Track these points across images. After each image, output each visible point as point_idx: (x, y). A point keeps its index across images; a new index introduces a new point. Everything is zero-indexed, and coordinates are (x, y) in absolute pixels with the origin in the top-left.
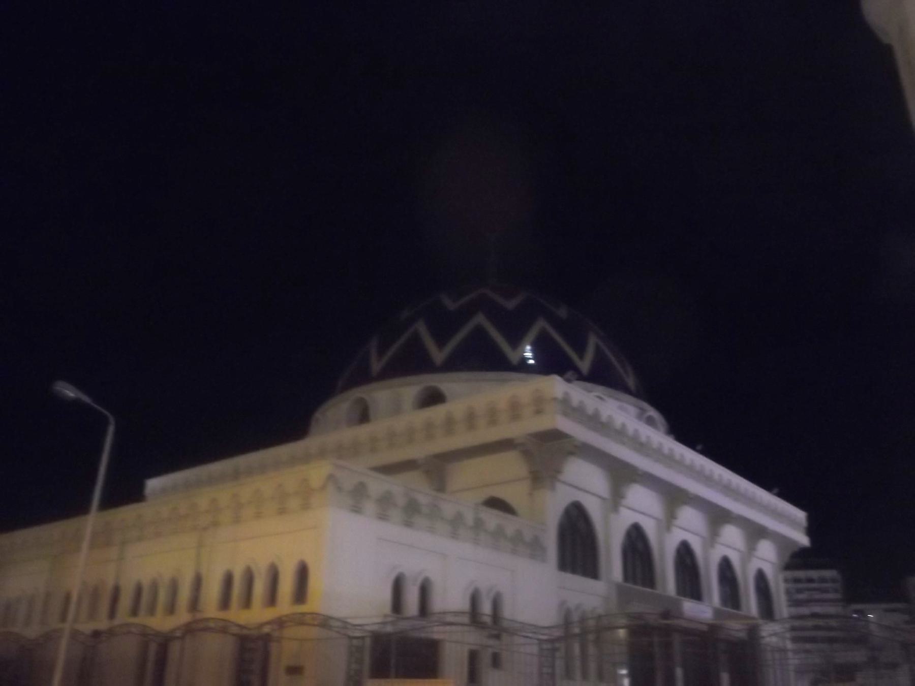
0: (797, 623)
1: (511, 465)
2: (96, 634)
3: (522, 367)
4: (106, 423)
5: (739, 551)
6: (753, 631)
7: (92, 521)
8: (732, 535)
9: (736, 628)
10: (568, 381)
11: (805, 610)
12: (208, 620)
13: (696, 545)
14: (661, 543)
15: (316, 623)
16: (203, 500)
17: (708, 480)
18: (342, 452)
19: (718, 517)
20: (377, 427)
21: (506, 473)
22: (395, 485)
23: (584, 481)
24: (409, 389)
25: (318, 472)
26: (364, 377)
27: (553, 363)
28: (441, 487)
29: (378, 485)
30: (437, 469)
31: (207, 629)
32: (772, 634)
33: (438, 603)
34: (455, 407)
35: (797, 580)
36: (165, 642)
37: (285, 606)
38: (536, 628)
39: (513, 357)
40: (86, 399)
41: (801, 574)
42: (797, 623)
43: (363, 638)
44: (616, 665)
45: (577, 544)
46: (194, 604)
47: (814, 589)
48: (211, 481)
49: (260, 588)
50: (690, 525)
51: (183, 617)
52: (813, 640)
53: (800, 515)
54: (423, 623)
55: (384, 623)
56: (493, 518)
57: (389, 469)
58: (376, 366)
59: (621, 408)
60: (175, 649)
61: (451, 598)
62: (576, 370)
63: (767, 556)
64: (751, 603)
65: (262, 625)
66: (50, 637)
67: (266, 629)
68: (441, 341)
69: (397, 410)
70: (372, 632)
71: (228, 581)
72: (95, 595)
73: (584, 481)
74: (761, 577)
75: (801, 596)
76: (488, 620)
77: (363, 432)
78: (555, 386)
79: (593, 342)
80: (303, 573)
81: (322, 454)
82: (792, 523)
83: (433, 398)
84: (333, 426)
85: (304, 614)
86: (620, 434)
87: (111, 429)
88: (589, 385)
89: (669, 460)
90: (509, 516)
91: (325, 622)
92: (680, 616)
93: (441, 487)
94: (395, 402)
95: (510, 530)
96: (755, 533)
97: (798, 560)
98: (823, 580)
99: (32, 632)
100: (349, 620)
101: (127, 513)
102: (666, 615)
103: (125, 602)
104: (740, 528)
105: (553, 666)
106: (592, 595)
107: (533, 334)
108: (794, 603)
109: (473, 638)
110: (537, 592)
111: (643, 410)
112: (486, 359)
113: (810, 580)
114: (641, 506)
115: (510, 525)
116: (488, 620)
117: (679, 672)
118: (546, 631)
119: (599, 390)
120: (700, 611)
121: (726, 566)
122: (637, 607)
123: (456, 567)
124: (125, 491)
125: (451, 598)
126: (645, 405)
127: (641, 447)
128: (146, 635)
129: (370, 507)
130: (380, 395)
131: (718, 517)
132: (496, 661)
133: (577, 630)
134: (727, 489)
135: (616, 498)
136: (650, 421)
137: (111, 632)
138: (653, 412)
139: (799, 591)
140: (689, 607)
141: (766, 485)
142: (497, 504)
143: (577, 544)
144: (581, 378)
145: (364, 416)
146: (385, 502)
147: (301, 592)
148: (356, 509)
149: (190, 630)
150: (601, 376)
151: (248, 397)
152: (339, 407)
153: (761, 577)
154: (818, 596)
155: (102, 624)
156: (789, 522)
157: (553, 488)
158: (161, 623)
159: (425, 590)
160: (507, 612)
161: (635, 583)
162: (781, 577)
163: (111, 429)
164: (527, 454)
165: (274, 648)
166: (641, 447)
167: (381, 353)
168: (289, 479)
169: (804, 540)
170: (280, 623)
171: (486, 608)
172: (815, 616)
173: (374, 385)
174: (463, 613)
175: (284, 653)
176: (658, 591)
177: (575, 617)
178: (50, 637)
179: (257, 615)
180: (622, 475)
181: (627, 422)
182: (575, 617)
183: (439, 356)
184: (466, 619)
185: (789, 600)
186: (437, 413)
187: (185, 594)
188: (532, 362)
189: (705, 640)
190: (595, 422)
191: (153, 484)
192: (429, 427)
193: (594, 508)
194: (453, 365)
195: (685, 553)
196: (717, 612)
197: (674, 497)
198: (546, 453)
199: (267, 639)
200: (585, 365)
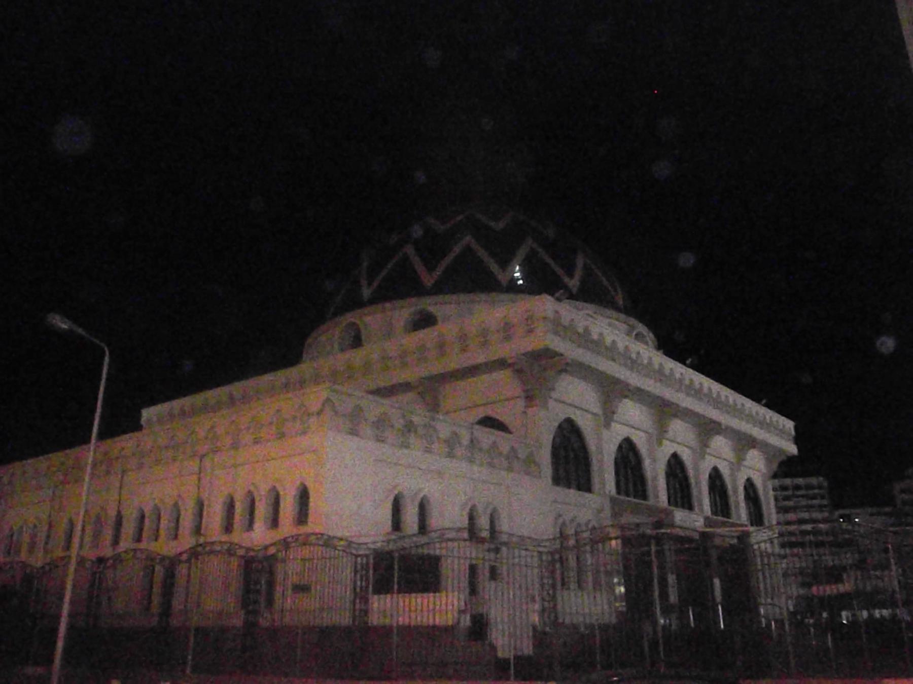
0: (784, 528)
1: (504, 382)
2: (101, 560)
3: (512, 288)
4: (104, 352)
5: (759, 471)
6: (743, 537)
7: (90, 453)
8: (720, 444)
9: (725, 535)
10: (559, 300)
11: (791, 516)
12: (213, 543)
13: (686, 456)
14: (734, 481)
15: (321, 543)
16: (202, 425)
17: (698, 393)
18: (334, 376)
19: (707, 429)
20: (371, 351)
21: (499, 391)
22: (384, 406)
23: (575, 398)
24: (402, 312)
25: (315, 396)
26: (355, 303)
27: (541, 282)
28: (434, 407)
29: (375, 408)
30: (431, 390)
31: (212, 552)
32: (763, 540)
33: (435, 521)
34: (447, 329)
35: (784, 488)
36: (171, 565)
37: (287, 528)
38: (538, 543)
39: (502, 278)
40: (80, 331)
41: (788, 481)
42: (784, 528)
43: (367, 556)
44: (609, 574)
45: (570, 459)
46: (198, 530)
47: (802, 496)
48: (206, 408)
49: (262, 510)
50: (680, 438)
51: (187, 541)
52: (802, 545)
53: (789, 425)
54: (423, 540)
55: (388, 541)
56: (487, 437)
57: (389, 392)
58: (366, 292)
59: (610, 325)
60: (182, 569)
61: (449, 515)
62: (565, 287)
63: (756, 466)
64: (741, 512)
65: (266, 548)
66: (55, 566)
67: (272, 550)
68: (431, 269)
69: (389, 334)
70: (374, 549)
71: (230, 507)
72: (99, 522)
73: (575, 398)
74: (750, 485)
75: (790, 503)
76: (485, 534)
77: (357, 356)
78: (545, 305)
79: (580, 262)
80: (304, 496)
81: (317, 379)
82: (781, 432)
83: (425, 321)
84: (326, 351)
85: (308, 535)
86: (611, 352)
87: (107, 359)
88: (580, 304)
89: (661, 375)
90: (503, 434)
91: (328, 542)
92: (672, 525)
93: (434, 407)
94: (387, 329)
95: (505, 448)
96: (744, 443)
97: (786, 468)
98: (809, 487)
99: (38, 560)
100: (354, 540)
101: (127, 443)
102: (659, 525)
103: (129, 528)
104: (730, 440)
105: (554, 578)
106: (590, 508)
107: (522, 253)
108: (781, 510)
109: (472, 552)
110: (532, 508)
111: (632, 328)
112: (475, 280)
113: (797, 487)
114: (633, 420)
115: (504, 442)
116: (485, 534)
117: (671, 579)
118: (547, 544)
119: (590, 308)
120: (692, 521)
121: (716, 477)
122: (629, 519)
123: (450, 485)
124: (123, 421)
125: (449, 515)
126: (633, 321)
127: (633, 364)
128: (151, 560)
129: (368, 431)
130: (371, 320)
131: (707, 429)
132: (494, 574)
133: (572, 542)
134: (717, 403)
135: (608, 416)
136: (639, 337)
137: (118, 559)
138: (641, 328)
139: (787, 498)
140: (680, 516)
141: (758, 400)
142: (489, 422)
143: (570, 459)
144: (572, 297)
145: (357, 342)
146: (381, 423)
147: (302, 516)
148: (354, 432)
149: (194, 553)
150: (591, 294)
151: (241, 323)
152: (330, 335)
153: (750, 485)
154: (804, 502)
155: (108, 552)
156: (778, 433)
157: (545, 406)
158: (165, 547)
159: (423, 508)
160: (504, 525)
161: (628, 495)
162: (770, 484)
163: (107, 359)
164: (519, 372)
165: (279, 567)
166: (633, 364)
167: (370, 284)
168: (287, 403)
169: (793, 449)
170: (285, 544)
171: (483, 522)
172: (801, 522)
173: (366, 311)
174: (459, 530)
175: (290, 571)
176: (651, 502)
177: (570, 531)
178: (55, 566)
179: (260, 535)
180: (612, 391)
181: (617, 339)
182: (570, 531)
183: (428, 280)
184: (466, 535)
185: (777, 507)
186: (427, 335)
187: (187, 521)
188: (521, 282)
189: (696, 549)
190: (584, 340)
191: (147, 414)
192: (422, 348)
193: (585, 423)
194: (438, 289)
195: (716, 477)
196: (708, 522)
197: (664, 411)
198: (537, 371)
199: (272, 560)
200: (574, 283)
